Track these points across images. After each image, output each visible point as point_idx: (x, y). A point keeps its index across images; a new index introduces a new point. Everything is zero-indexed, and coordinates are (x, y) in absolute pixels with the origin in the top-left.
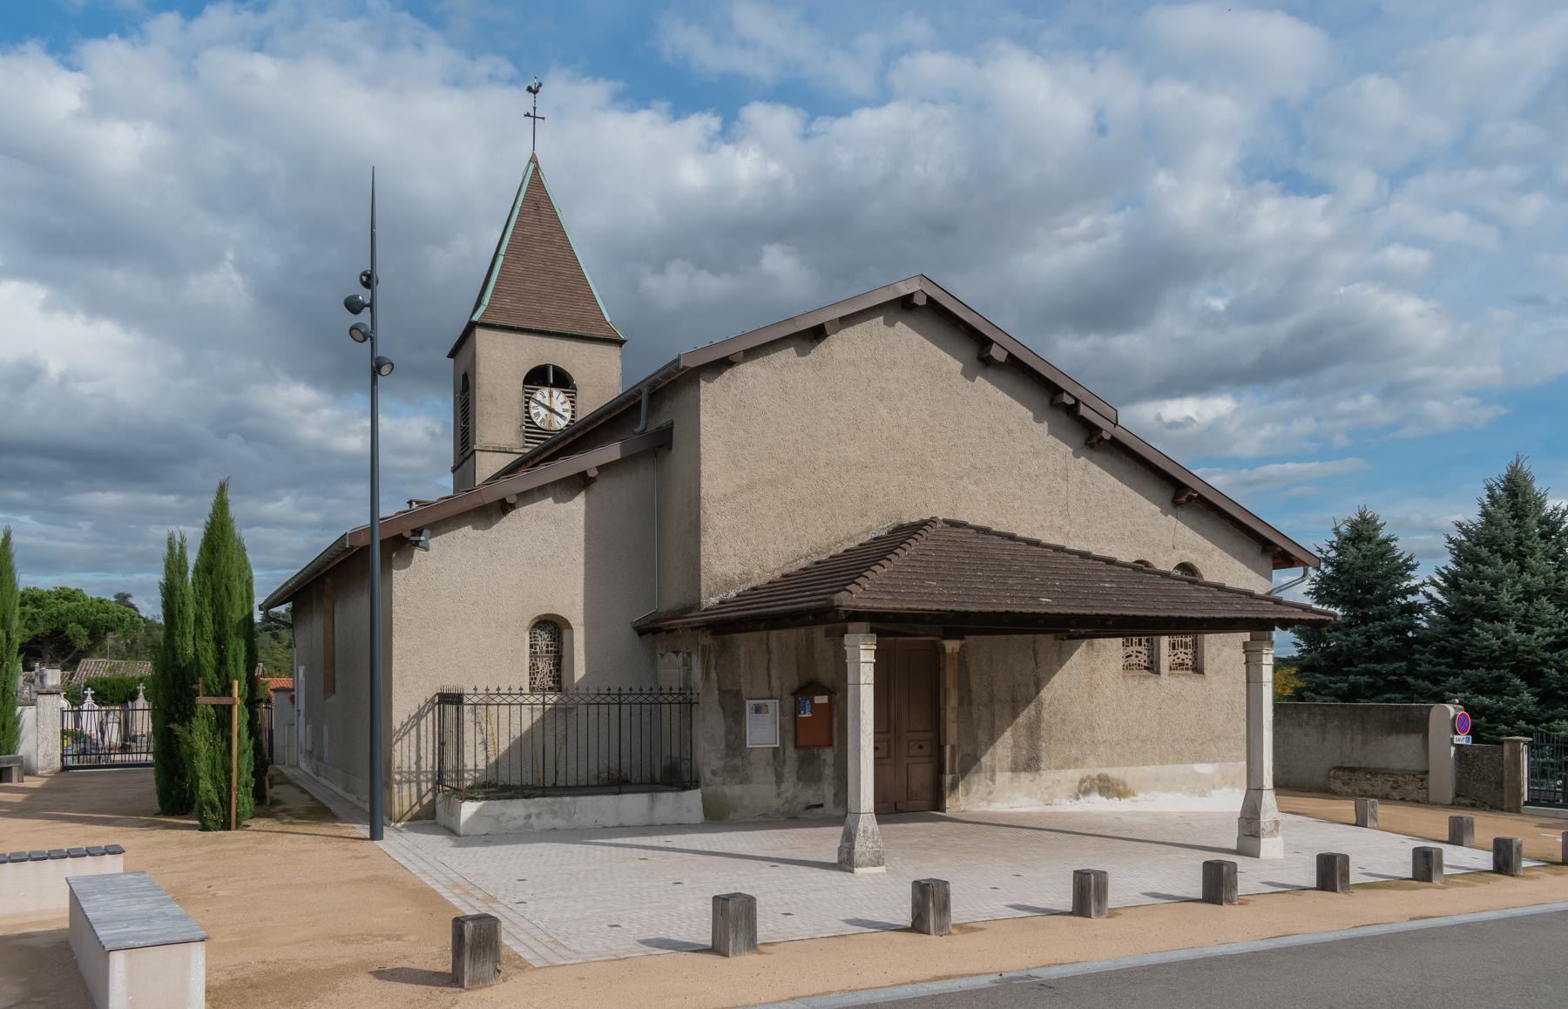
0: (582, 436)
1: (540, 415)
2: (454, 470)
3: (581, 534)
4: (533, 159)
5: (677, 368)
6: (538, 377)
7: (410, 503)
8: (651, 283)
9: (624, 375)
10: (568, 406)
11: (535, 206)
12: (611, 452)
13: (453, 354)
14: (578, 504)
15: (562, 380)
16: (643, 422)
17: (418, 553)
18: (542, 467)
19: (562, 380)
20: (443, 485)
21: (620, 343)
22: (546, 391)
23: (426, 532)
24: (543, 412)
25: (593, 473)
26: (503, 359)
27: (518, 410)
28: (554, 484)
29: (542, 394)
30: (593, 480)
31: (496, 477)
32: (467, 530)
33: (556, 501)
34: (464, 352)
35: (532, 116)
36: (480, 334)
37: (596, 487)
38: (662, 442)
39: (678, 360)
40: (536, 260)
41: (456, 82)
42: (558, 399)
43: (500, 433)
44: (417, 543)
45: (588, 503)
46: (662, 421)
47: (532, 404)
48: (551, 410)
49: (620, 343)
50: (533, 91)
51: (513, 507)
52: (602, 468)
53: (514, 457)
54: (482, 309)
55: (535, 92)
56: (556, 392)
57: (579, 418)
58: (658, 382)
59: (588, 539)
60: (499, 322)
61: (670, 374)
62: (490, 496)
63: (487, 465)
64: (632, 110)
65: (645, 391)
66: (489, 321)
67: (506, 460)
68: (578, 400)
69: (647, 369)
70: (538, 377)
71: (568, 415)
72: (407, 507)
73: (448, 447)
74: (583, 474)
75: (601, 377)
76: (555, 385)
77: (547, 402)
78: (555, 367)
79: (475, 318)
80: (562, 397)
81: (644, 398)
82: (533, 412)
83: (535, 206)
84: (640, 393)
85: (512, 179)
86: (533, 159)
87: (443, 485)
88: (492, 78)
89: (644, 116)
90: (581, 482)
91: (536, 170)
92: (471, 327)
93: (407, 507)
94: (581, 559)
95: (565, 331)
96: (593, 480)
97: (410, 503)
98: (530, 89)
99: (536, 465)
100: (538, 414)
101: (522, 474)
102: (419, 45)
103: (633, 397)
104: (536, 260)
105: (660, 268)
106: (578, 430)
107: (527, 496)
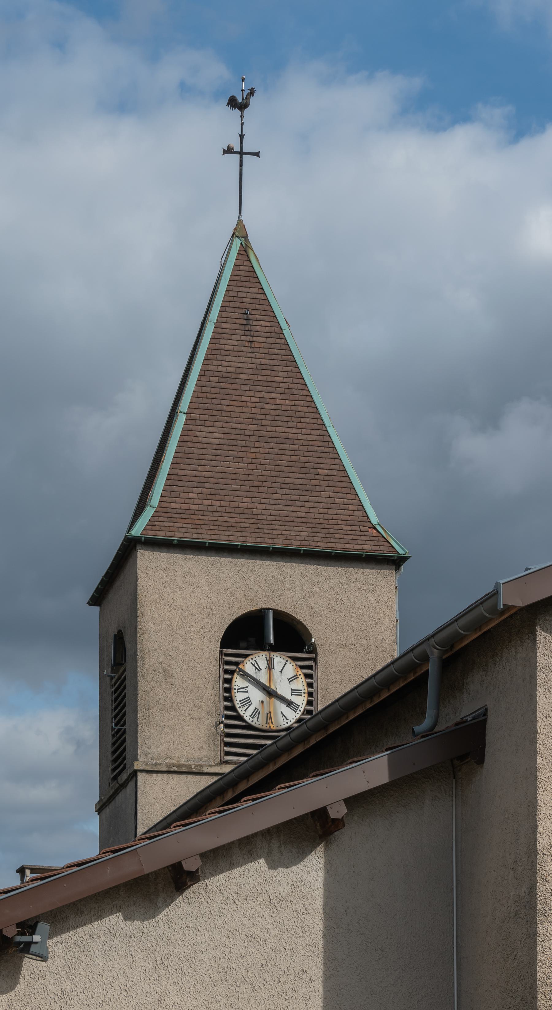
0: (326, 739)
1: (249, 700)
2: (100, 808)
3: (316, 924)
4: (240, 232)
5: (494, 610)
6: (248, 633)
7: (21, 871)
8: (472, 446)
9: (404, 622)
10: (301, 684)
11: (244, 312)
12: (372, 771)
13: (98, 598)
14: (312, 870)
15: (291, 637)
16: (430, 712)
17: (29, 965)
18: (244, 805)
19: (291, 637)
20: (79, 839)
21: (396, 562)
22: (261, 658)
23: (43, 927)
24: (256, 695)
25: (338, 811)
26: (185, 602)
27: (212, 695)
28: (268, 833)
29: (256, 663)
30: (338, 824)
31: (166, 823)
32: (114, 921)
33: (272, 866)
34: (117, 596)
35: (238, 152)
36: (145, 559)
37: (344, 837)
38: (465, 750)
39: (494, 594)
40: (247, 422)
41: (123, 103)
42: (284, 673)
43: (180, 740)
44: (26, 948)
45: (329, 867)
46: (466, 709)
47: (238, 682)
48: (270, 693)
49: (396, 562)
50: (238, 104)
51: (194, 877)
52: (354, 802)
53: (204, 782)
54: (148, 514)
55: (242, 107)
56: (279, 659)
57: (320, 705)
58: (457, 638)
59: (330, 934)
60: (178, 536)
61: (480, 622)
62: (153, 858)
63: (158, 798)
64: (438, 127)
65: (435, 654)
66: (160, 535)
67: (188, 788)
68: (320, 672)
69: (446, 606)
70: (248, 633)
71: (301, 701)
72: (14, 881)
73: (91, 765)
74: (321, 814)
75: (361, 626)
76: (277, 647)
77: (263, 678)
78: (278, 614)
79: (137, 530)
80: (291, 669)
81: (432, 668)
82: (238, 697)
83: (244, 312)
84: (425, 658)
85: (207, 265)
86: (240, 232)
87: (79, 839)
88: (186, 90)
89: (462, 138)
90: (316, 828)
91: (245, 251)
92: (129, 548)
93: (14, 881)
94: (316, 970)
95: (295, 545)
96: (338, 824)
97: (21, 871)
98: (232, 103)
99: (236, 800)
100: (247, 702)
101: (210, 817)
102: (60, 45)
103: (412, 667)
104: (247, 422)
105: (490, 419)
106: (322, 726)
107: (221, 857)
